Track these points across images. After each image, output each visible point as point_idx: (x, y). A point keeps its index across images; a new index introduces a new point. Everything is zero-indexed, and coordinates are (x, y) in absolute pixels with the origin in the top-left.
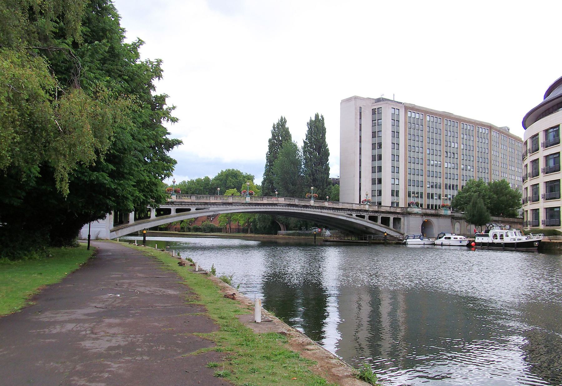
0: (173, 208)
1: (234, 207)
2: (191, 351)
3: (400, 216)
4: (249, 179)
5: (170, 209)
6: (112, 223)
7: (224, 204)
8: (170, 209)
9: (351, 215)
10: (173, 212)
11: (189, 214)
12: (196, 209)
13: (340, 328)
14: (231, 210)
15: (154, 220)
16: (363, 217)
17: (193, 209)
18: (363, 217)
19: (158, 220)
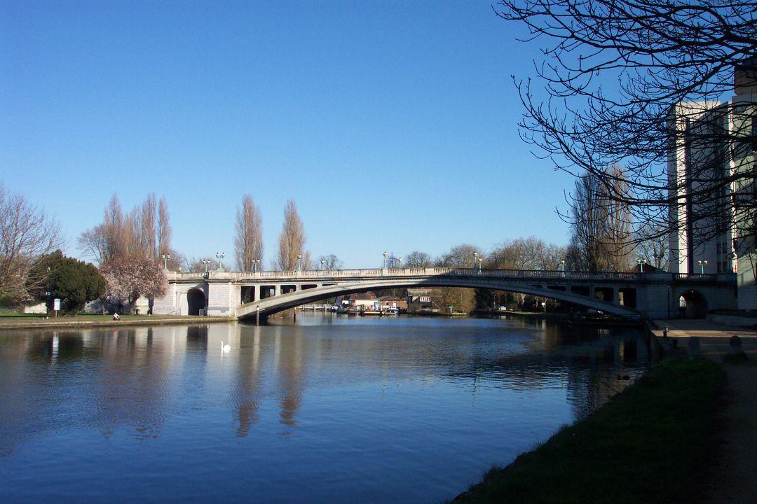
0: (298, 285)
1: (366, 282)
2: (689, 204)
3: (632, 286)
4: (392, 262)
5: (295, 286)
6: (240, 298)
7: (360, 279)
8: (254, 287)
9: (541, 287)
10: (298, 289)
11: (316, 291)
12: (323, 285)
13: (694, 341)
14: (363, 284)
15: (278, 298)
16: (563, 289)
17: (320, 285)
18: (563, 289)
19: (304, 293)
